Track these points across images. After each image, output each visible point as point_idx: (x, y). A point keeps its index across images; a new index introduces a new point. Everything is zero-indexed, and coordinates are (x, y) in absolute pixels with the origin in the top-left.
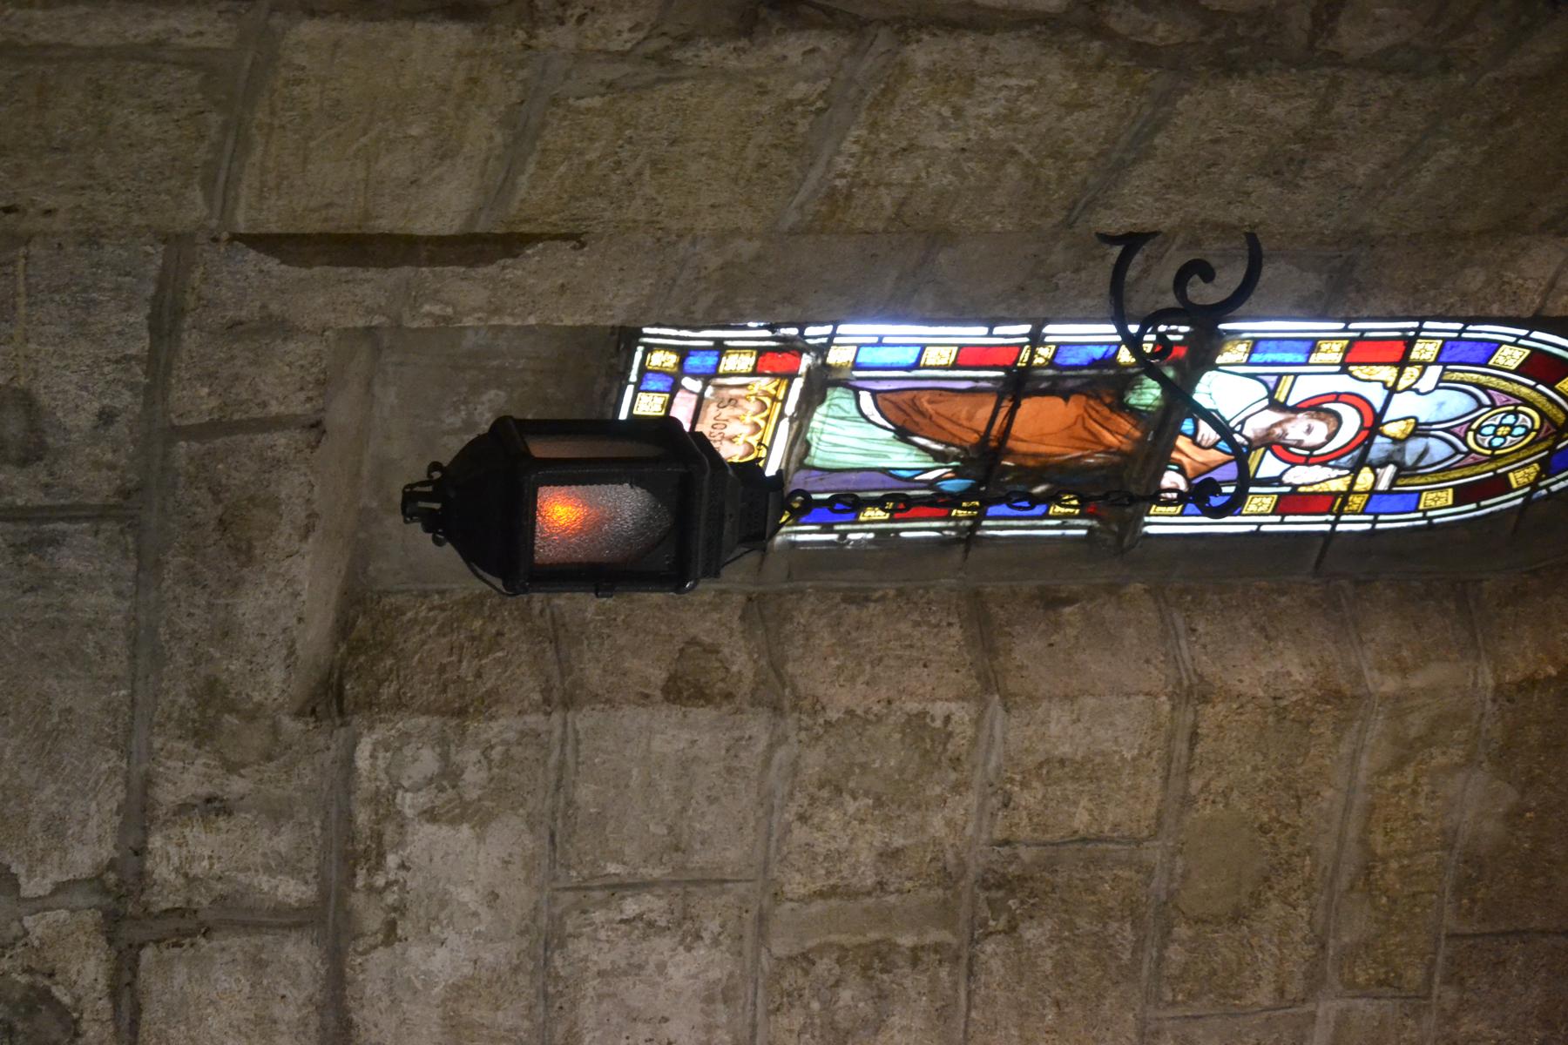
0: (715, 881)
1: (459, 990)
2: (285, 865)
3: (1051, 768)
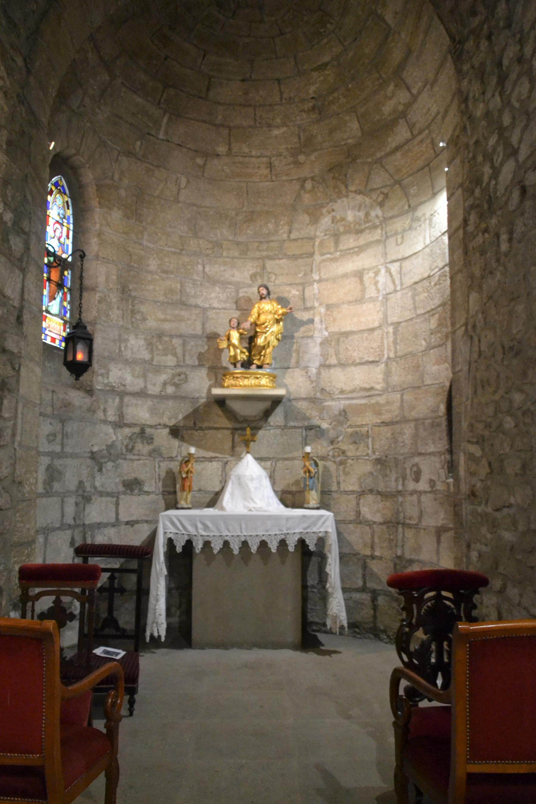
0: (120, 336)
1: (133, 376)
2: (114, 400)
3: (107, 281)
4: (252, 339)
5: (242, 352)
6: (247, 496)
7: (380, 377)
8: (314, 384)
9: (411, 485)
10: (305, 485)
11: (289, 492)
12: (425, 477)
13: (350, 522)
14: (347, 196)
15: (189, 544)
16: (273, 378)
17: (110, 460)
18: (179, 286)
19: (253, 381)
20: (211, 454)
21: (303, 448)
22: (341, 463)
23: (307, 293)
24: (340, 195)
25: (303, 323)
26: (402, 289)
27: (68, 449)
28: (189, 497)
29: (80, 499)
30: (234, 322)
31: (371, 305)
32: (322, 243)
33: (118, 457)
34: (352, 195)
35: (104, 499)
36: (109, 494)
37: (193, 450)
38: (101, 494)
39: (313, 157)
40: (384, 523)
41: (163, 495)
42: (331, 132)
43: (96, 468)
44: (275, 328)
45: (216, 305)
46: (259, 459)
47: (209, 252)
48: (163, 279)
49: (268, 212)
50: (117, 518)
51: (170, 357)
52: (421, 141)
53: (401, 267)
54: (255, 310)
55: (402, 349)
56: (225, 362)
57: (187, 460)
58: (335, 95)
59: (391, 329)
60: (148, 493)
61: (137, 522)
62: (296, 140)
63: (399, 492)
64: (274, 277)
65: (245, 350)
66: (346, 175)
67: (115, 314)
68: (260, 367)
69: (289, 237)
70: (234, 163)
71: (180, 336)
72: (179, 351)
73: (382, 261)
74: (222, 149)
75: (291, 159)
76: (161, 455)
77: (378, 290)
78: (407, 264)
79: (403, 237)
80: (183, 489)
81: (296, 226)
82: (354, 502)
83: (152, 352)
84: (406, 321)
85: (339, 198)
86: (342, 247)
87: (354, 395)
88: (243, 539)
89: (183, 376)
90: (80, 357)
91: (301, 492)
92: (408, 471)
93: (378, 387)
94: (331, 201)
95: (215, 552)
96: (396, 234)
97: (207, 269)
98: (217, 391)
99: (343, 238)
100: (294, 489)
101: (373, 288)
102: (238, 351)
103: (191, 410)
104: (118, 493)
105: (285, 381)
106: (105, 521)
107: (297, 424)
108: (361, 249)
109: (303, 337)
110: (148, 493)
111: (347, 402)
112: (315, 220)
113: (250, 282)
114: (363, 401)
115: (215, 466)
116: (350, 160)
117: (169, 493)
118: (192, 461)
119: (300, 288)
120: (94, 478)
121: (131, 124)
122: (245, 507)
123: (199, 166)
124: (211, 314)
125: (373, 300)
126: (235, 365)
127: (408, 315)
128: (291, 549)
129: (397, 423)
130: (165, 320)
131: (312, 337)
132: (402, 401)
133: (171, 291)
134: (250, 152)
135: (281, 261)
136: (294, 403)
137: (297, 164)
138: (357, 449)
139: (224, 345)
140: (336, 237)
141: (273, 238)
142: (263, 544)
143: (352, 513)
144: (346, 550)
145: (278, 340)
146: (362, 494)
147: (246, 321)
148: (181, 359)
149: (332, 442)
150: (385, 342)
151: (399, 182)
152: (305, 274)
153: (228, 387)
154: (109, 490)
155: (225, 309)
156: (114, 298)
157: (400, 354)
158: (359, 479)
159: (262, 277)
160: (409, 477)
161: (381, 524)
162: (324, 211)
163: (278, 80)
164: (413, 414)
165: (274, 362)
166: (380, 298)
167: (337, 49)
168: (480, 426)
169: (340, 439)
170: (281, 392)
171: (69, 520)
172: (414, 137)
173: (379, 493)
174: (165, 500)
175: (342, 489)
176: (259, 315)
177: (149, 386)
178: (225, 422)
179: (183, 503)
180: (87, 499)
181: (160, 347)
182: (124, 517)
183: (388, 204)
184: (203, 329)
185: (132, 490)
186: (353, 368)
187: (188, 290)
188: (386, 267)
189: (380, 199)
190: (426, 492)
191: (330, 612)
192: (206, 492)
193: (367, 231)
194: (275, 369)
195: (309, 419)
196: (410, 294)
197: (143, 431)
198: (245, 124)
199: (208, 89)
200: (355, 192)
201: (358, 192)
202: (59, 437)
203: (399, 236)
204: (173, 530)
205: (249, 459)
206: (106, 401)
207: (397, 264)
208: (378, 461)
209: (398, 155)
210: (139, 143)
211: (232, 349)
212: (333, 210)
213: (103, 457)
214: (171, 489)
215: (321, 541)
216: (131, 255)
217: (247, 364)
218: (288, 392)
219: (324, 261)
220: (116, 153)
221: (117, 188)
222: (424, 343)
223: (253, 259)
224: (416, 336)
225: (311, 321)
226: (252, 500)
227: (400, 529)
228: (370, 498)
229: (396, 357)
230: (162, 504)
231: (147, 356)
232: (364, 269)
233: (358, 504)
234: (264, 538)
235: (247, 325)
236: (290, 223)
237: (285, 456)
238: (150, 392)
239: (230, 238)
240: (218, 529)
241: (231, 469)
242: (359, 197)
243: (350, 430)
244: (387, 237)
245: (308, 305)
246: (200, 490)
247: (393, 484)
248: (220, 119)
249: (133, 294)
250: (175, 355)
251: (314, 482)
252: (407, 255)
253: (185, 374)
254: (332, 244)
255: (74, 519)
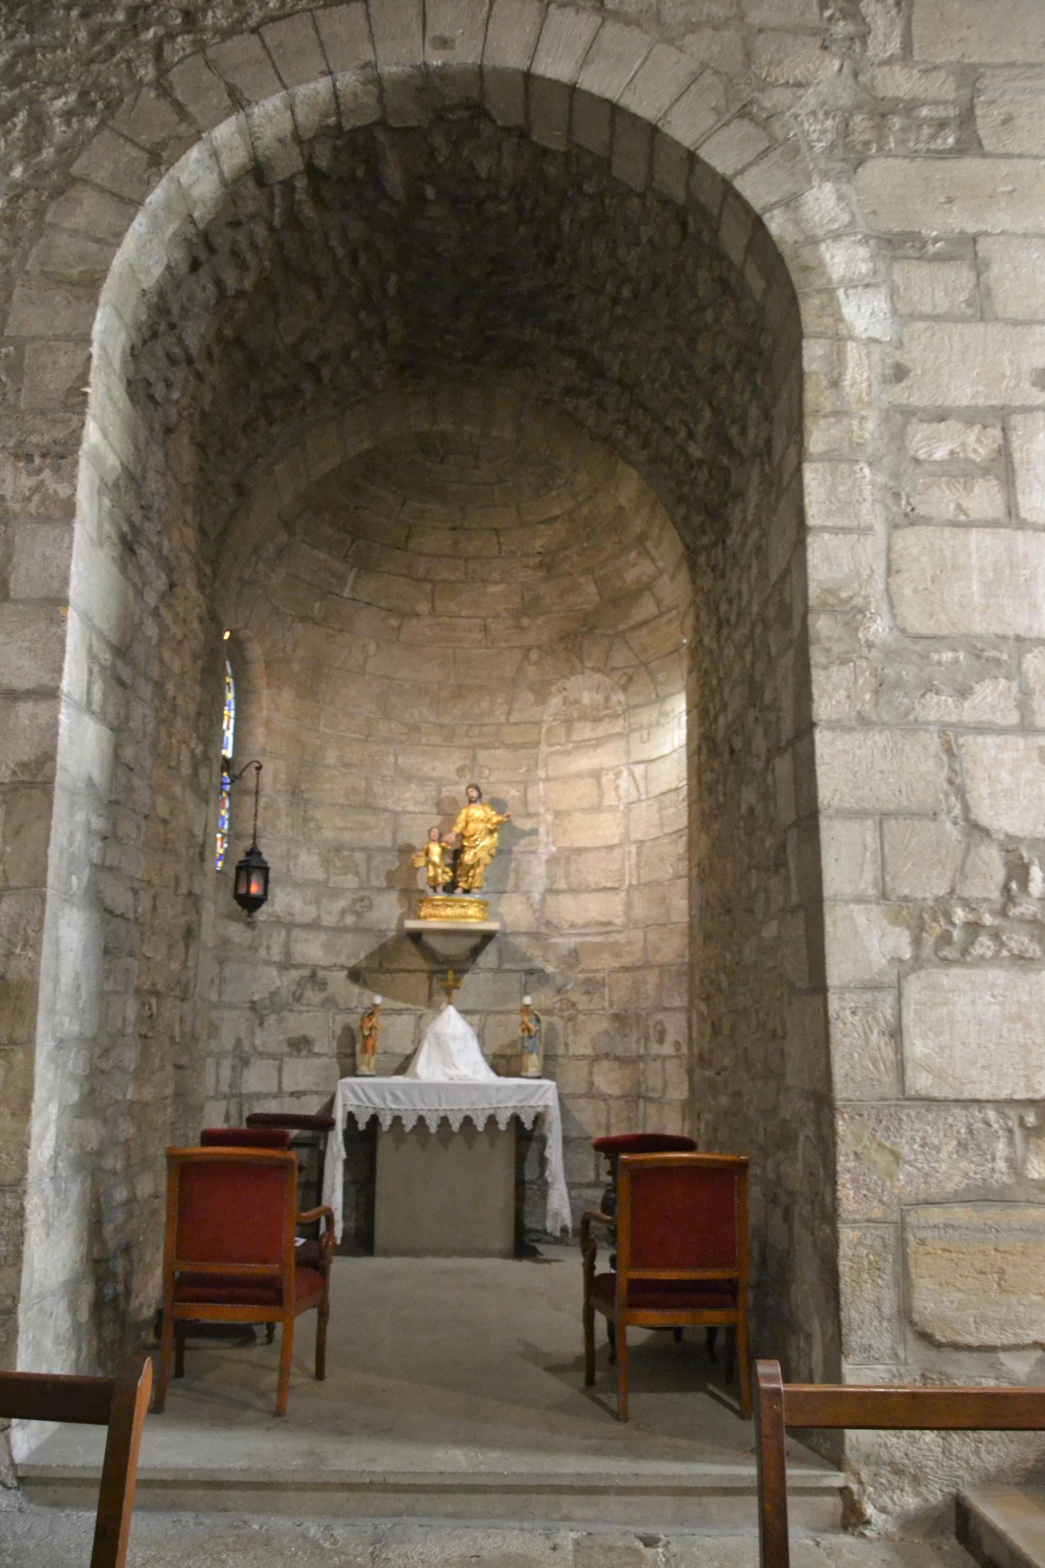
0: (289, 850)
1: (304, 902)
2: (279, 936)
3: (274, 782)
4: (457, 853)
5: (444, 872)
6: (447, 1059)
7: (620, 908)
8: (537, 915)
9: (655, 1048)
10: (523, 1047)
11: (503, 1057)
12: (670, 1038)
13: (581, 1096)
14: (582, 673)
15: (374, 1120)
16: (484, 905)
17: (273, 1012)
18: (363, 784)
19: (458, 911)
20: (400, 1005)
21: (521, 998)
22: (571, 1019)
23: (531, 794)
24: (573, 671)
25: (524, 834)
26: (647, 799)
27: (226, 998)
28: (373, 1061)
29: (237, 1061)
30: (435, 833)
31: (610, 816)
32: (549, 731)
33: (283, 1007)
34: (588, 672)
35: (265, 1062)
36: (272, 1056)
37: (378, 1000)
38: (262, 1055)
39: (540, 621)
40: (623, 1096)
41: (339, 1058)
42: (562, 594)
43: (257, 1022)
44: (488, 841)
45: (411, 807)
46: (464, 1012)
47: (404, 738)
48: (343, 775)
49: (480, 687)
50: (280, 1088)
51: (350, 877)
52: (670, 621)
53: (646, 771)
54: (462, 817)
55: (646, 875)
56: (422, 883)
57: (372, 1012)
58: (568, 552)
59: (633, 849)
60: (319, 1055)
61: (304, 1093)
62: (518, 599)
63: (640, 1057)
64: (487, 772)
65: (448, 870)
66: (581, 648)
67: (283, 823)
68: (466, 891)
69: (507, 719)
70: (438, 624)
71: (364, 849)
72: (362, 868)
73: (624, 760)
74: (423, 607)
75: (510, 622)
76: (336, 1005)
77: (618, 797)
78: (653, 767)
79: (649, 733)
80: (365, 1050)
81: (517, 705)
82: (586, 1070)
83: (327, 870)
84: (652, 840)
85: (572, 674)
86: (575, 737)
87: (587, 930)
88: (442, 1114)
89: (366, 902)
90: (255, 889)
91: (519, 1056)
92: (651, 1030)
93: (618, 921)
94: (563, 677)
95: (407, 1129)
96: (641, 728)
97: (400, 761)
98: (411, 924)
99: (578, 726)
100: (509, 1052)
101: (613, 794)
102: (440, 871)
103: (376, 946)
104: (282, 1054)
105: (499, 909)
106: (265, 1091)
107: (513, 967)
108: (599, 742)
109: (524, 853)
110: (319, 1055)
111: (579, 939)
112: (542, 699)
113: (455, 777)
114: (599, 939)
115: (407, 1020)
116: (584, 629)
117: (346, 1055)
118: (377, 1014)
119: (522, 787)
120: (253, 1034)
121: (310, 584)
122: (445, 1074)
123: (393, 628)
124: (404, 820)
125: (613, 809)
126: (434, 888)
127: (654, 832)
128: (502, 1127)
129: (639, 968)
130: (344, 829)
131: (534, 852)
132: (645, 940)
133: (354, 790)
134: (456, 543)
135: (498, 752)
136: (511, 939)
137: (520, 628)
138: (590, 1001)
139: (421, 862)
140: (569, 723)
141: (487, 721)
142: (468, 1121)
143: (584, 1085)
144: (574, 1134)
145: (491, 856)
146: (595, 1059)
147: (450, 831)
148: (364, 878)
149: (559, 991)
150: (627, 864)
151: (645, 664)
152: (528, 770)
153: (425, 917)
154: (271, 1050)
155: (422, 813)
156: (282, 803)
157: (643, 881)
158: (592, 1040)
159: (472, 771)
160: (652, 1038)
161: (618, 1098)
162: (554, 688)
163: (497, 531)
164: (658, 957)
165: (485, 884)
166: (622, 808)
167: (569, 504)
168: (707, 981)
169: (569, 987)
170: (493, 926)
171: (224, 1088)
172: (661, 614)
173: (617, 1058)
174: (341, 1064)
175: (571, 1053)
176: (467, 823)
177: (324, 916)
178: (418, 962)
179: (363, 1069)
180: (245, 1062)
181: (338, 864)
182: (288, 1086)
183: (631, 690)
184: (394, 839)
185: (299, 1051)
186: (587, 896)
187: (375, 788)
188: (629, 769)
189: (623, 681)
190: (672, 1057)
191: (549, 1207)
192: (394, 1055)
193: (607, 720)
194: (487, 893)
195: (530, 960)
196: (656, 806)
197: (314, 975)
198: (452, 578)
199: (408, 537)
200: (593, 669)
201: (598, 670)
202: (217, 983)
203: (645, 732)
204: (355, 1102)
205: (451, 1012)
206: (270, 936)
207: (642, 767)
208: (617, 1017)
209: (644, 631)
210: (318, 605)
211: (431, 868)
212: (565, 689)
213: (265, 1008)
214: (349, 1051)
215: (539, 1119)
216: (303, 746)
217: (450, 887)
218: (503, 924)
219: (552, 753)
220: (290, 618)
221: (289, 662)
222: (670, 870)
223: (460, 747)
224: (662, 860)
225: (535, 832)
226: (454, 1065)
227: (641, 1103)
228: (605, 1064)
229: (639, 884)
230: (336, 1070)
231: (321, 876)
232: (602, 769)
233: (591, 1073)
234: (469, 1113)
235: (451, 837)
236: (510, 702)
237: (499, 1008)
238: (324, 923)
239: (432, 719)
240: (412, 1101)
241: (427, 1025)
242: (598, 677)
243: (582, 976)
244: (631, 731)
245: (532, 810)
246: (385, 1052)
247: (634, 1047)
248: (421, 571)
249: (306, 796)
250: (357, 874)
251: (534, 1044)
252: (654, 756)
253: (369, 899)
254: (563, 733)
255: (230, 1086)
